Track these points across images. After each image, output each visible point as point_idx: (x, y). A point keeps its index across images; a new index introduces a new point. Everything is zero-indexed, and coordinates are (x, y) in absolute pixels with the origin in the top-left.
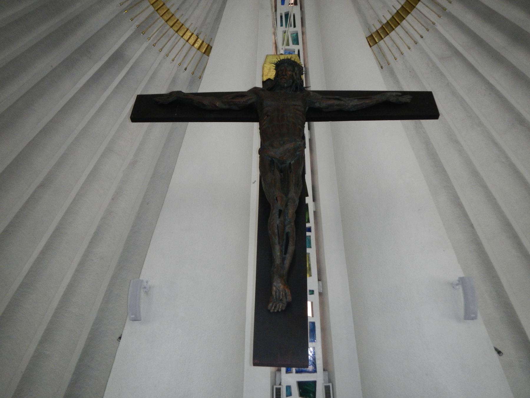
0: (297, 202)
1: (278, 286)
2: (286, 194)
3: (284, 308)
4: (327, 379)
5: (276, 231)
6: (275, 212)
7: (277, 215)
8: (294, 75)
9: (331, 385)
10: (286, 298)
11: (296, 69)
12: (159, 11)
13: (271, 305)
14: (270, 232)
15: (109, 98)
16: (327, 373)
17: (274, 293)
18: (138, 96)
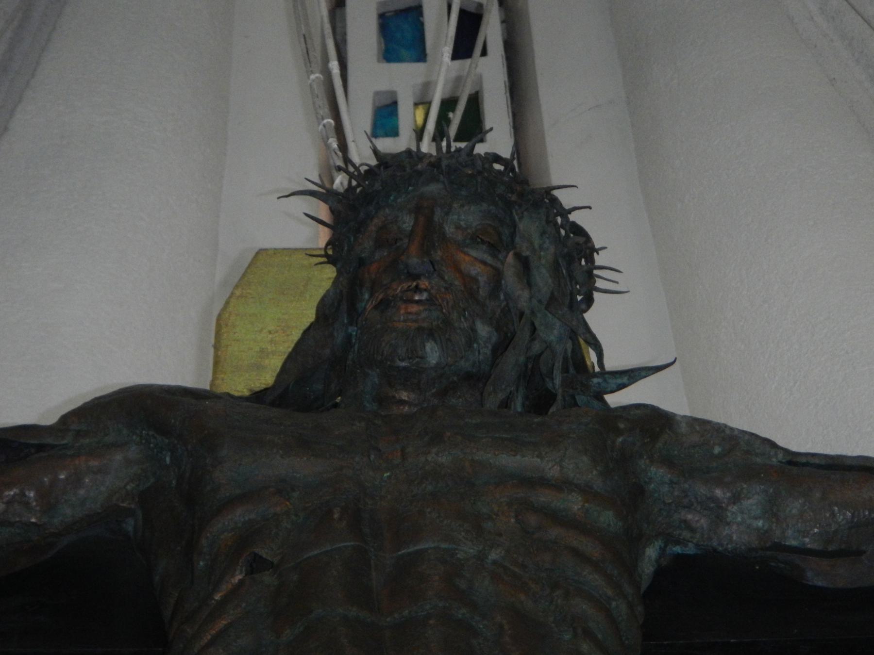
11: (529, 226)
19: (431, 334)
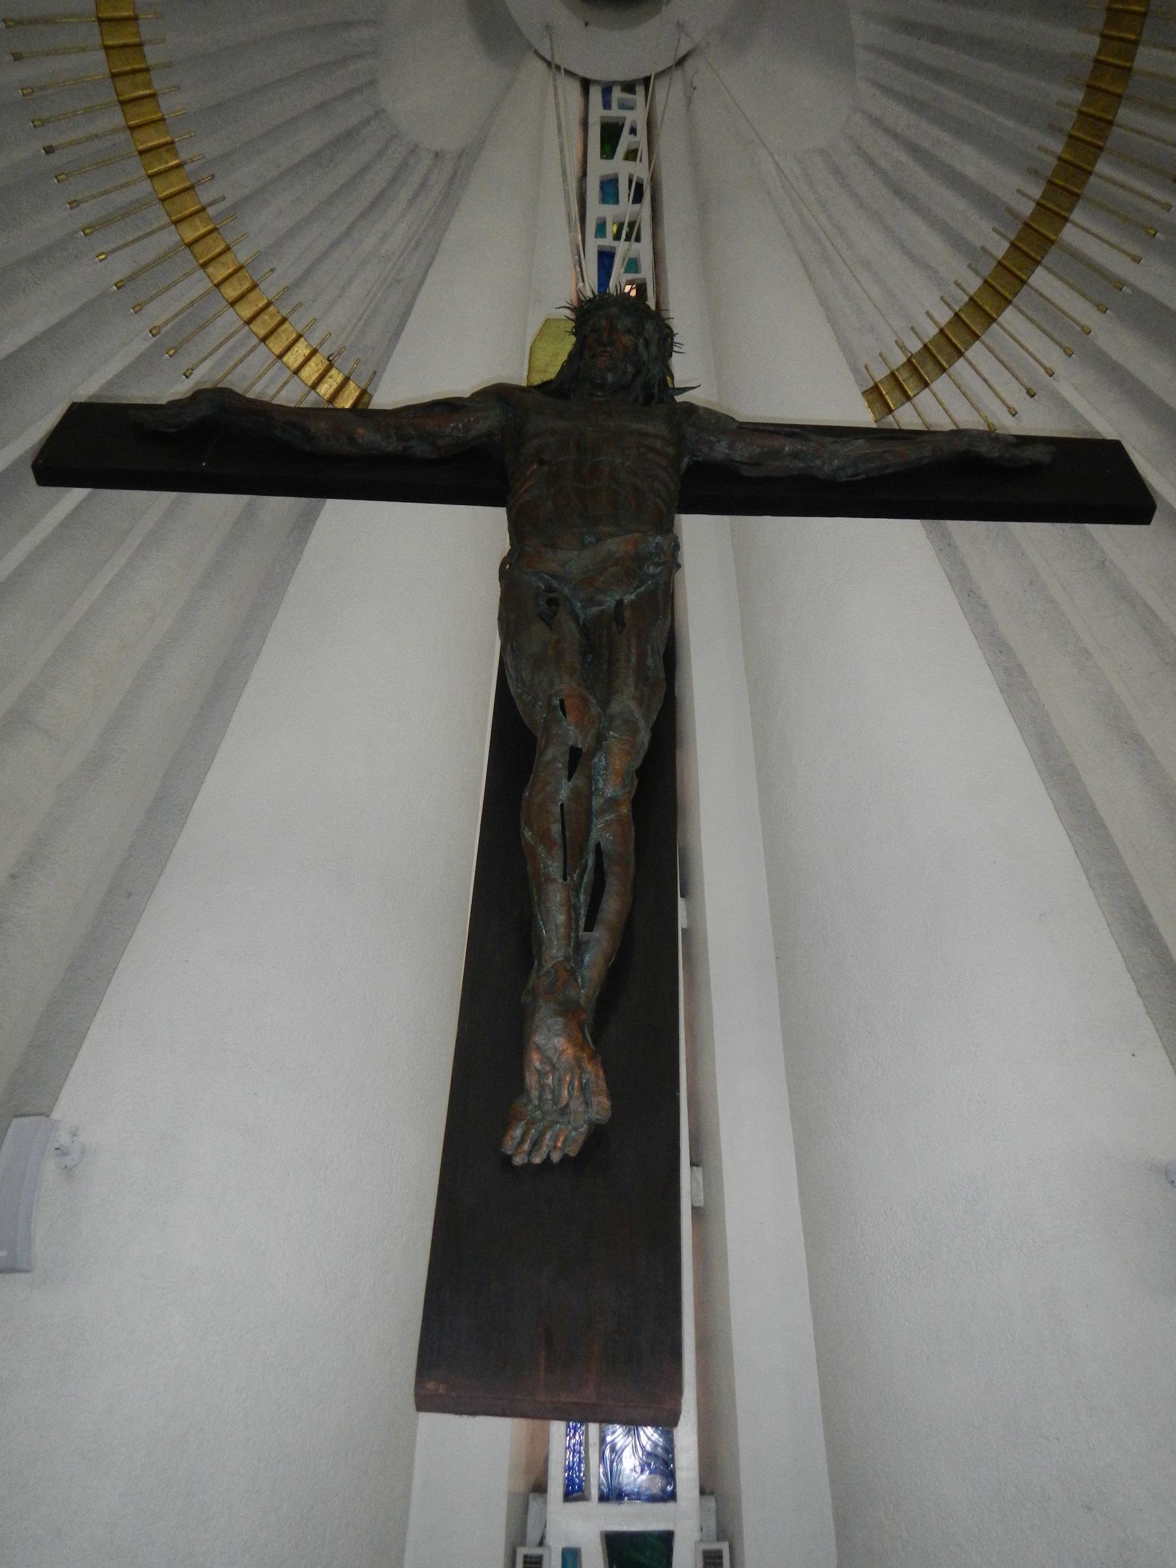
0: (645, 737)
1: (552, 1045)
2: (605, 703)
3: (573, 1151)
4: (712, 1524)
5: (556, 828)
6: (553, 756)
7: (561, 765)
8: (641, 349)
9: (724, 1547)
10: (587, 1104)
11: (649, 327)
12: (210, 270)
13: (518, 1133)
14: (528, 834)
15: (37, 557)
16: (711, 1503)
17: (531, 1080)
18: (73, 404)
19: (610, 370)
